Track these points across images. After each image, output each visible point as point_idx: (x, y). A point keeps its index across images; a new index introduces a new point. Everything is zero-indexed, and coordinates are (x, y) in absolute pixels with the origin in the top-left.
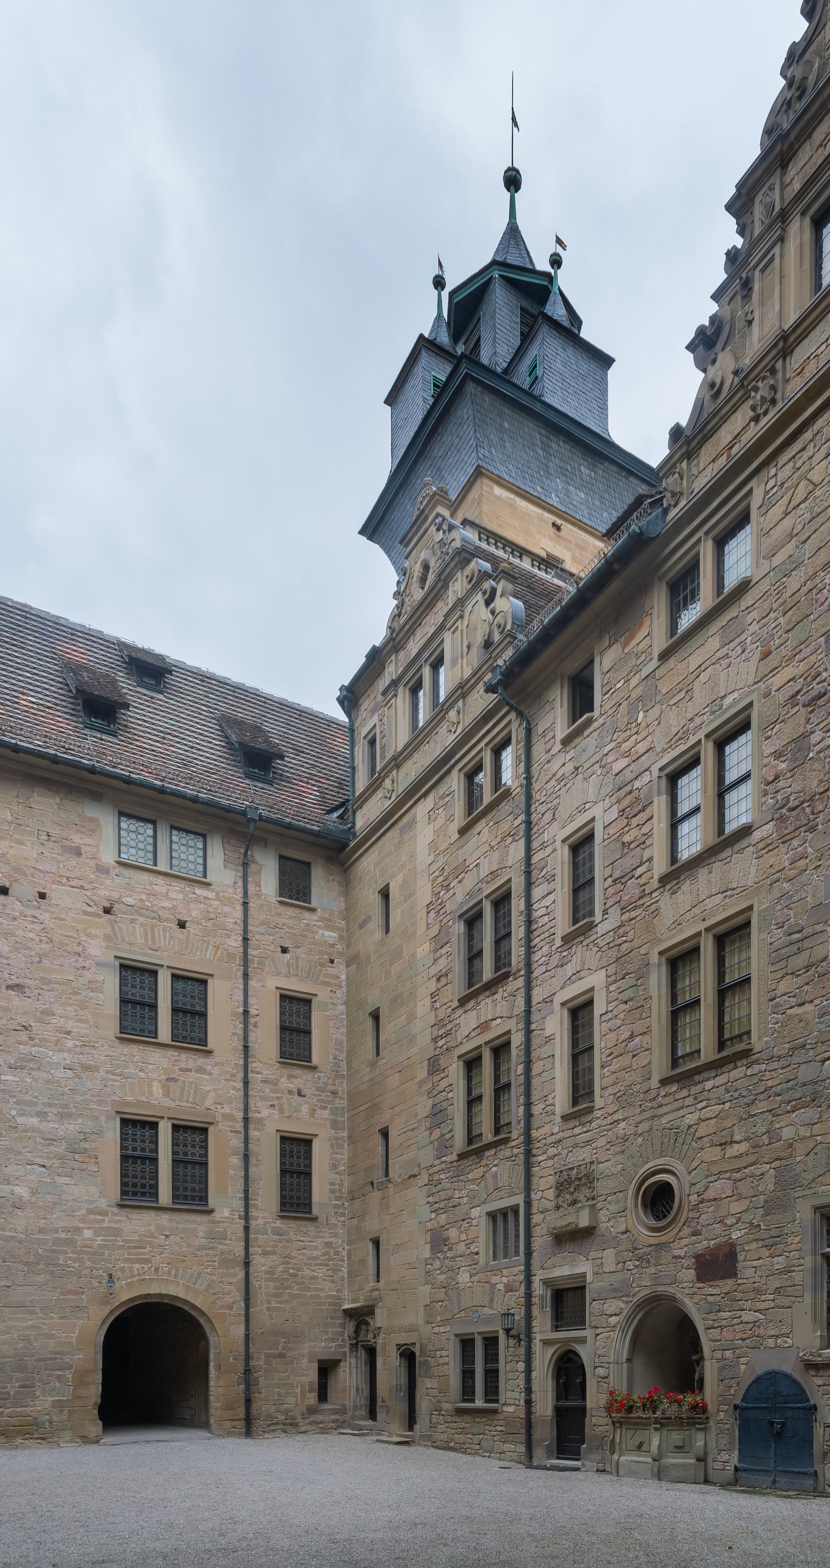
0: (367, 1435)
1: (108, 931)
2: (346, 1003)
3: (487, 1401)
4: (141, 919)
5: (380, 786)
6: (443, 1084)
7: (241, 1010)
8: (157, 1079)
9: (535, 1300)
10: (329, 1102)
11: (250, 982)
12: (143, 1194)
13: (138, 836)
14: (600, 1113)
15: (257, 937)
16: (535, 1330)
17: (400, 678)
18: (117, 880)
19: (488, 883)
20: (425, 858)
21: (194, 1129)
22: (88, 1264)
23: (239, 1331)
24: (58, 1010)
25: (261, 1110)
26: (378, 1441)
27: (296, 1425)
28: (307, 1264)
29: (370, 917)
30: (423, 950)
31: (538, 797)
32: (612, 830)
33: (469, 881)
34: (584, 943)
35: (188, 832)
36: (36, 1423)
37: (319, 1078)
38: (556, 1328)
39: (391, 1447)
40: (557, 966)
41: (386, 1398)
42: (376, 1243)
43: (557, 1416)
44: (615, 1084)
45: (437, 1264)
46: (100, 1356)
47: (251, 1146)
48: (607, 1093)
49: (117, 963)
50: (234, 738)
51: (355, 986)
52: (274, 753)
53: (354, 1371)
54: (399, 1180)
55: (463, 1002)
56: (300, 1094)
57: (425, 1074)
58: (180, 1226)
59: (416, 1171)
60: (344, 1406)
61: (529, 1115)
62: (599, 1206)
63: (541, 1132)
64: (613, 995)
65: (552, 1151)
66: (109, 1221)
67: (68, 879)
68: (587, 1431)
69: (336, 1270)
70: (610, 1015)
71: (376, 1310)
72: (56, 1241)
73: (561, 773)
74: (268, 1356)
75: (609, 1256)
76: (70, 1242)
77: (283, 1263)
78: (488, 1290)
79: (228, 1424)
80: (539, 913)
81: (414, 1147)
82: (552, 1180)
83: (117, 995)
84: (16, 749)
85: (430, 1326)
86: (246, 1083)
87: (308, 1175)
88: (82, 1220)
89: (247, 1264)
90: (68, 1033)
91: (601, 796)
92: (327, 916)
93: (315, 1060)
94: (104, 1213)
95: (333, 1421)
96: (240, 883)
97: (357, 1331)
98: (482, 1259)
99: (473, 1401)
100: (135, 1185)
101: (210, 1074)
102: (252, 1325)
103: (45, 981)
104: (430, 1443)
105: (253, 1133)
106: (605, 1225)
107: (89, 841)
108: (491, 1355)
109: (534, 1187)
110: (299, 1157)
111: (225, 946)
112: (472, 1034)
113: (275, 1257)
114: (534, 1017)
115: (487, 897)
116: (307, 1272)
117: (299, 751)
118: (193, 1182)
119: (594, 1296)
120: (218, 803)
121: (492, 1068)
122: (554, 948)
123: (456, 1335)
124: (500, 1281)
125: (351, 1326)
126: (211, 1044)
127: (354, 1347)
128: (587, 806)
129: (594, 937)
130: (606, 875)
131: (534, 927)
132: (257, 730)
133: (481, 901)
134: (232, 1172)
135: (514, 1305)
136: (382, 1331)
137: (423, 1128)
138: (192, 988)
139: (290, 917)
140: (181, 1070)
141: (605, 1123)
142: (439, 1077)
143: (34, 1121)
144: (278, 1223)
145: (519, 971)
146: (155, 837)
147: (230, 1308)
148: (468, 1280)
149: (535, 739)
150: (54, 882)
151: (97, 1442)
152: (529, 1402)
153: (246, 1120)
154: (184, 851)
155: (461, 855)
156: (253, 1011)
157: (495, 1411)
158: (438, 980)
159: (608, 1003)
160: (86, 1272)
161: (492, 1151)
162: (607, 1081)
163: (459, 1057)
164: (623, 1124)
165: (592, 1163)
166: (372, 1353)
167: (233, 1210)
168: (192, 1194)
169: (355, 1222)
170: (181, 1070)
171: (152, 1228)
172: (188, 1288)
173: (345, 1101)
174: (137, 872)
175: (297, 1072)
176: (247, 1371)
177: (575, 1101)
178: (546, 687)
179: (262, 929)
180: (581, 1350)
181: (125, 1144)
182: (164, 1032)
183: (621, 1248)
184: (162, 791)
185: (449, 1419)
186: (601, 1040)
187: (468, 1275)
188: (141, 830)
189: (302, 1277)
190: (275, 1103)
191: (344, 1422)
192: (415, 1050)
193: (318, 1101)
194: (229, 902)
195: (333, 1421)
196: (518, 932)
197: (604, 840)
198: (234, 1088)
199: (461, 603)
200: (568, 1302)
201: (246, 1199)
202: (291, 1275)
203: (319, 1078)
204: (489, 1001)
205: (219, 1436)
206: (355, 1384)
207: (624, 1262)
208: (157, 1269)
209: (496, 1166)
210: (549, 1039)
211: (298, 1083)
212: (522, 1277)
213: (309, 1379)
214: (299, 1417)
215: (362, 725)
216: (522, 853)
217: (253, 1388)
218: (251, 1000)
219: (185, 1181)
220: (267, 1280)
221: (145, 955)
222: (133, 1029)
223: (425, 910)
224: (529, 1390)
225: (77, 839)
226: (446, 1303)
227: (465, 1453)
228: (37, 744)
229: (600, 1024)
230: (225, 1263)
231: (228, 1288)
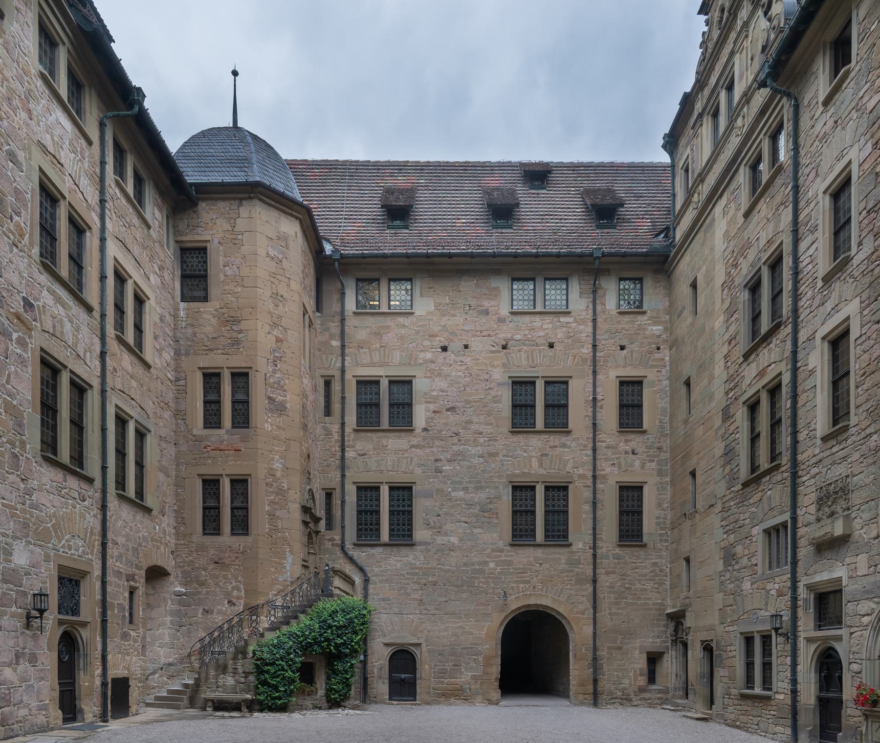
0: (681, 711)
1: (505, 361)
2: (669, 378)
3: (764, 689)
4: (525, 348)
5: (690, 202)
6: (732, 428)
7: (591, 398)
8: (535, 457)
9: (800, 603)
10: (656, 456)
11: (598, 377)
12: (527, 536)
13: (523, 291)
14: (855, 429)
15: (603, 342)
16: (800, 629)
17: (704, 110)
18: (511, 325)
19: (765, 251)
20: (721, 249)
21: (403, 488)
22: (492, 585)
23: (589, 630)
24: (475, 419)
25: (605, 468)
26: (684, 716)
27: (630, 700)
28: (639, 580)
29: (684, 307)
30: (719, 322)
31: (804, 162)
32: (866, 166)
33: (752, 255)
34: (842, 278)
35: (555, 279)
36: (462, 689)
37: (648, 439)
38: (819, 627)
39: (690, 721)
40: (819, 306)
41: (694, 683)
42: (688, 560)
43: (820, 705)
44: (868, 400)
45: (728, 575)
46: (499, 646)
47: (598, 496)
48: (861, 410)
49: (510, 382)
50: (589, 203)
51: (675, 362)
52: (616, 204)
53: (674, 661)
54: (703, 510)
55: (746, 356)
56: (633, 453)
57: (720, 422)
58: (549, 557)
59: (713, 501)
60: (667, 688)
61: (795, 442)
62: (853, 515)
63: (805, 455)
64: (867, 318)
65: (815, 471)
66: (505, 556)
67: (481, 332)
68: (843, 720)
69: (661, 584)
70: (863, 338)
71: (687, 614)
72: (474, 571)
73: (823, 131)
74: (609, 648)
75: (862, 561)
76: (481, 571)
77: (621, 580)
78: (764, 597)
79: (581, 697)
80: (804, 264)
81: (714, 483)
82: (813, 497)
83: (510, 403)
84: (450, 256)
85: (722, 626)
86: (594, 450)
87: (640, 513)
88: (489, 556)
89: (595, 581)
90: (481, 433)
91: (857, 138)
92: (655, 315)
93: (646, 425)
94: (502, 551)
95: (658, 699)
96: (591, 306)
97: (676, 630)
98: (759, 569)
99: (753, 688)
100: (521, 530)
101: (570, 447)
102: (598, 625)
103: (467, 402)
104: (722, 721)
105: (600, 486)
106: (858, 532)
107: (493, 303)
108: (767, 651)
109: (799, 505)
110: (633, 500)
111: (580, 354)
112: (754, 382)
113: (615, 576)
114: (800, 356)
115: (764, 264)
116: (638, 586)
117: (638, 197)
118: (559, 525)
119: (849, 598)
120: (574, 252)
121: (771, 406)
122: (816, 291)
123: (741, 633)
124: (773, 587)
125: (672, 626)
126: (571, 426)
127: (674, 642)
128: (845, 152)
129: (851, 269)
130: (861, 209)
131: (800, 276)
132: (610, 191)
133: (760, 268)
134: (584, 516)
135: (783, 607)
136: (692, 630)
137: (718, 466)
138: (558, 387)
139: (628, 322)
140: (550, 447)
141: (859, 438)
142: (729, 423)
143: (461, 494)
144: (617, 551)
145: (788, 319)
146: (534, 289)
147: (583, 613)
148: (749, 587)
149: (802, 110)
150: (473, 336)
151: (497, 704)
152: (794, 692)
153: (594, 477)
154: (554, 293)
155: (746, 235)
156: (599, 397)
157: (769, 698)
158: (730, 343)
159: (862, 326)
160: (491, 590)
161: (767, 478)
162: (860, 400)
163: (744, 403)
164: (875, 437)
165: (847, 476)
166: (685, 645)
167: (585, 544)
168: (558, 534)
169: (674, 546)
170: (550, 447)
171: (532, 559)
172: (554, 600)
173: (668, 454)
174: (523, 316)
175: (631, 436)
176: (595, 659)
177: (835, 422)
178: (811, 61)
179: (606, 336)
180: (837, 646)
181: (360, 503)
182: (540, 424)
183: (873, 553)
184: (537, 255)
185: (736, 702)
186: (856, 362)
187: (749, 583)
188: (526, 287)
189: (635, 590)
190: (615, 462)
191: (667, 699)
192: (713, 404)
193: (648, 456)
194: (583, 322)
195: (658, 699)
196: (787, 286)
197: (859, 178)
198: (586, 455)
199: (746, 24)
200: (827, 604)
201: (594, 534)
202: (627, 588)
203: (648, 439)
204: (765, 351)
205: (575, 705)
206: (675, 671)
207: (876, 566)
208: (534, 587)
209: (770, 489)
210: (812, 372)
211: (633, 445)
212: (789, 584)
213: (640, 666)
214: (632, 694)
215: (680, 159)
216: (790, 217)
217: (599, 672)
218: (598, 390)
219: (554, 525)
220: (609, 592)
221: (527, 372)
222: (521, 424)
223: (720, 289)
224: (794, 681)
225: (486, 304)
226: (734, 607)
227: (747, 731)
228: (463, 248)
229: (855, 348)
230: (580, 581)
231: (582, 599)
